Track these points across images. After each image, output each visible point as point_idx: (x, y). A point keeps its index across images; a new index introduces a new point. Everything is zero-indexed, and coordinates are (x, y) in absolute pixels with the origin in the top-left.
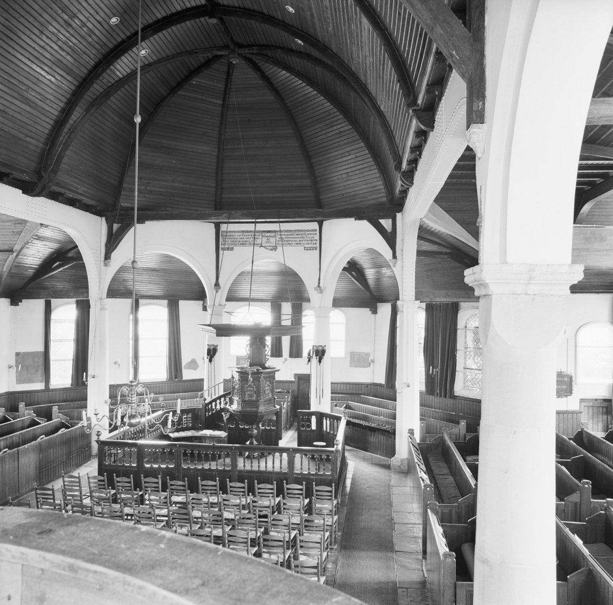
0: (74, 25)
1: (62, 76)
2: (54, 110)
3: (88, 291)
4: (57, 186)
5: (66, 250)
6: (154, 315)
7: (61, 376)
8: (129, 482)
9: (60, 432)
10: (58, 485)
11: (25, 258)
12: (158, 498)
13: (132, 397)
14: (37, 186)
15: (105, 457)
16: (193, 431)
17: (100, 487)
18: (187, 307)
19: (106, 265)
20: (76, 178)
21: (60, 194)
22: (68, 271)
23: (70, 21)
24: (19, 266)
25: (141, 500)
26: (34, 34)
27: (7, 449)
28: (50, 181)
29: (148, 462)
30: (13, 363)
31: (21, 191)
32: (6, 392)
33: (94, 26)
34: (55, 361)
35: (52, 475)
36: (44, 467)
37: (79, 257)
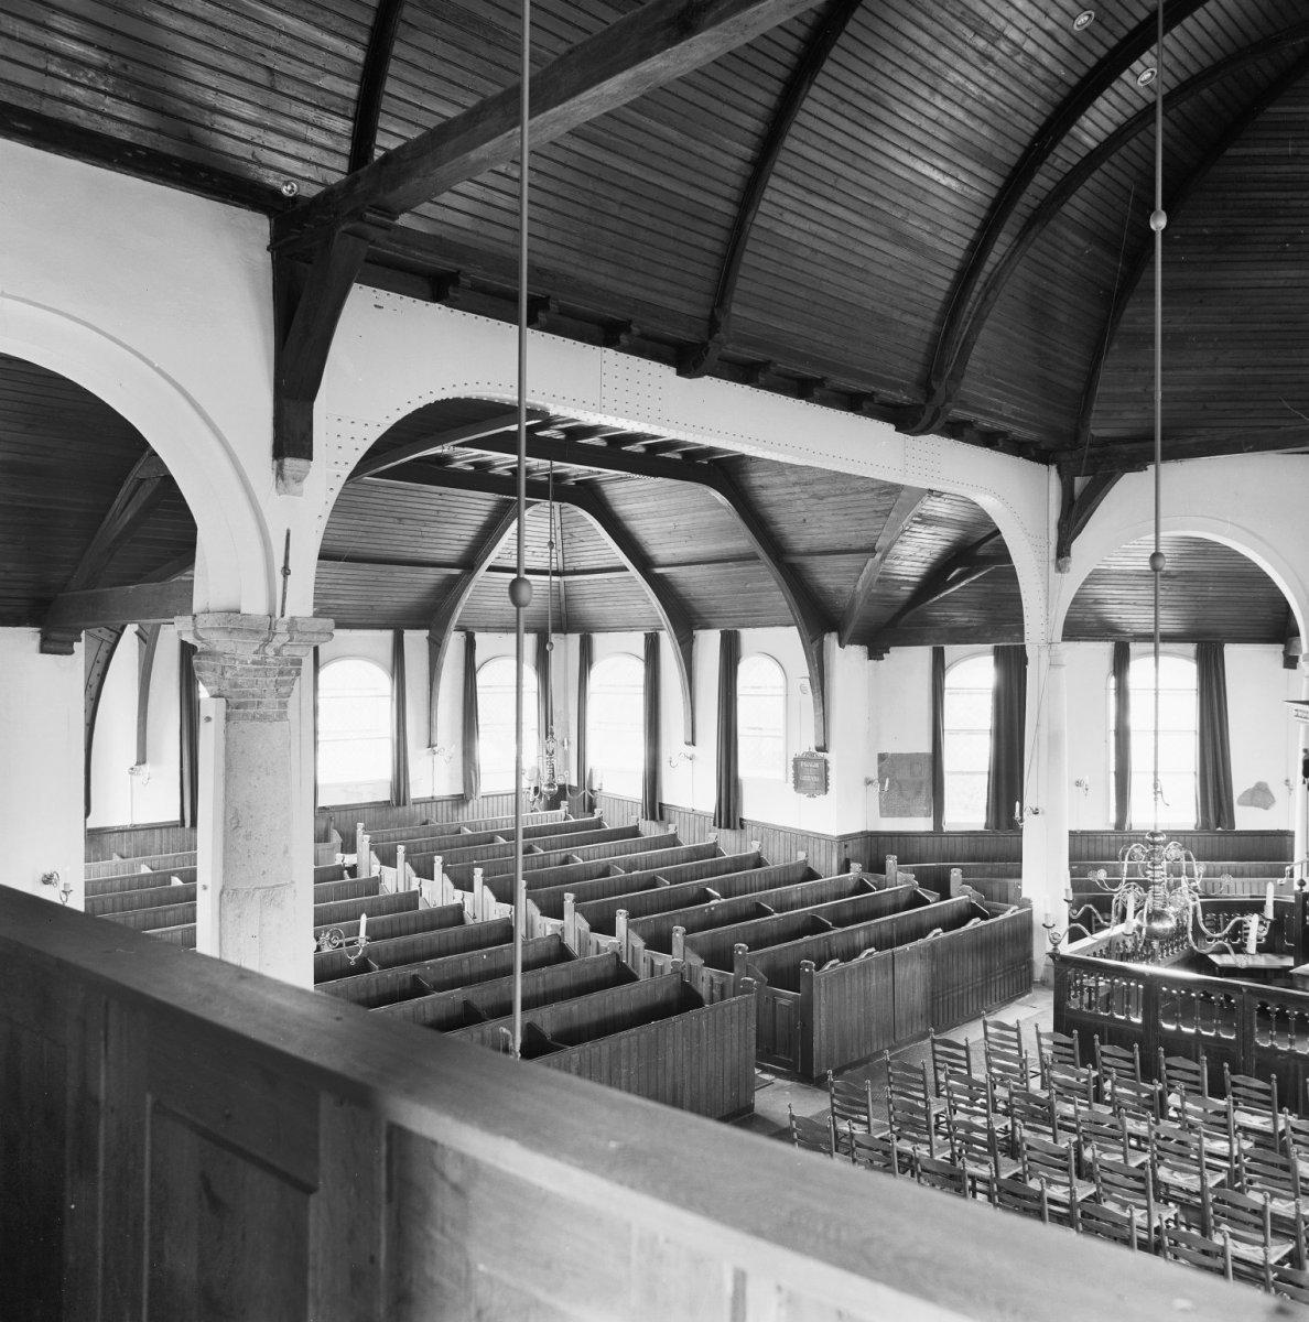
0: (998, 56)
1: (970, 173)
2: (953, 246)
3: (1023, 628)
4: (960, 408)
5: (975, 541)
6: (1165, 682)
7: (967, 808)
8: (1132, 1061)
9: (970, 925)
10: (971, 1034)
11: (897, 562)
12: (1200, 1109)
13: (1154, 870)
14: (923, 413)
15: (1069, 991)
16: (1269, 956)
17: (1061, 1058)
18: (1246, 663)
19: (1059, 569)
20: (997, 386)
21: (968, 424)
22: (978, 585)
23: (991, 49)
24: (886, 581)
25: (1158, 1107)
26: (920, 97)
27: (873, 949)
28: (948, 398)
29: (1170, 1018)
30: (874, 775)
31: (892, 427)
32: (862, 833)
33: (1039, 45)
34: (953, 773)
35: (956, 1015)
36: (941, 994)
37: (1002, 555)
